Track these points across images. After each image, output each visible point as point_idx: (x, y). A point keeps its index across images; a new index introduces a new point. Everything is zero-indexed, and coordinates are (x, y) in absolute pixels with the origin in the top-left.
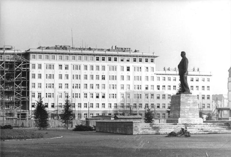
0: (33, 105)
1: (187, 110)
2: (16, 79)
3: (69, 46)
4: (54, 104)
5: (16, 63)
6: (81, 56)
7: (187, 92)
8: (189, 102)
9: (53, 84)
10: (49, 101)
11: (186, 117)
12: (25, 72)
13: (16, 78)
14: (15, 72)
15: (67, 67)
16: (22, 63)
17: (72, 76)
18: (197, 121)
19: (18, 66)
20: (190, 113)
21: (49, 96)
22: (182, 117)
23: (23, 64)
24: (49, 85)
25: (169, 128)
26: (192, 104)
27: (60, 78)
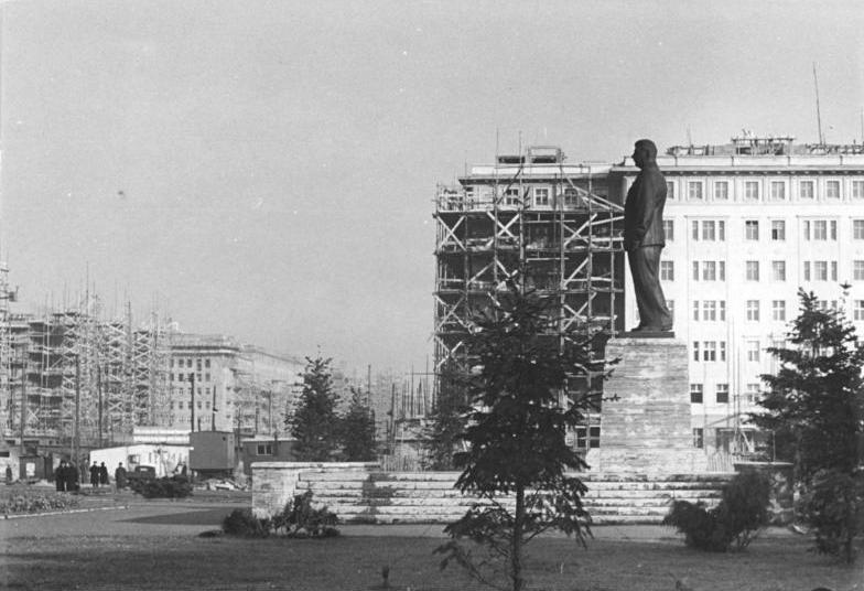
0: (697, 391)
1: (636, 411)
2: (570, 283)
3: (787, 139)
4: (726, 387)
5: (568, 216)
6: (838, 178)
7: (657, 330)
8: (644, 374)
9: (723, 304)
10: (705, 377)
11: (633, 443)
12: (608, 254)
13: (567, 281)
14: (566, 255)
15: (779, 228)
16: (592, 218)
17: (803, 269)
18: (679, 461)
19: (505, 224)
20: (647, 428)
21: (706, 353)
22: (609, 445)
23: (594, 220)
24: (706, 306)
25: (445, 497)
26: (659, 386)
27: (749, 277)
